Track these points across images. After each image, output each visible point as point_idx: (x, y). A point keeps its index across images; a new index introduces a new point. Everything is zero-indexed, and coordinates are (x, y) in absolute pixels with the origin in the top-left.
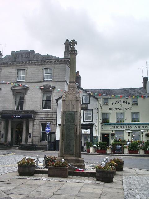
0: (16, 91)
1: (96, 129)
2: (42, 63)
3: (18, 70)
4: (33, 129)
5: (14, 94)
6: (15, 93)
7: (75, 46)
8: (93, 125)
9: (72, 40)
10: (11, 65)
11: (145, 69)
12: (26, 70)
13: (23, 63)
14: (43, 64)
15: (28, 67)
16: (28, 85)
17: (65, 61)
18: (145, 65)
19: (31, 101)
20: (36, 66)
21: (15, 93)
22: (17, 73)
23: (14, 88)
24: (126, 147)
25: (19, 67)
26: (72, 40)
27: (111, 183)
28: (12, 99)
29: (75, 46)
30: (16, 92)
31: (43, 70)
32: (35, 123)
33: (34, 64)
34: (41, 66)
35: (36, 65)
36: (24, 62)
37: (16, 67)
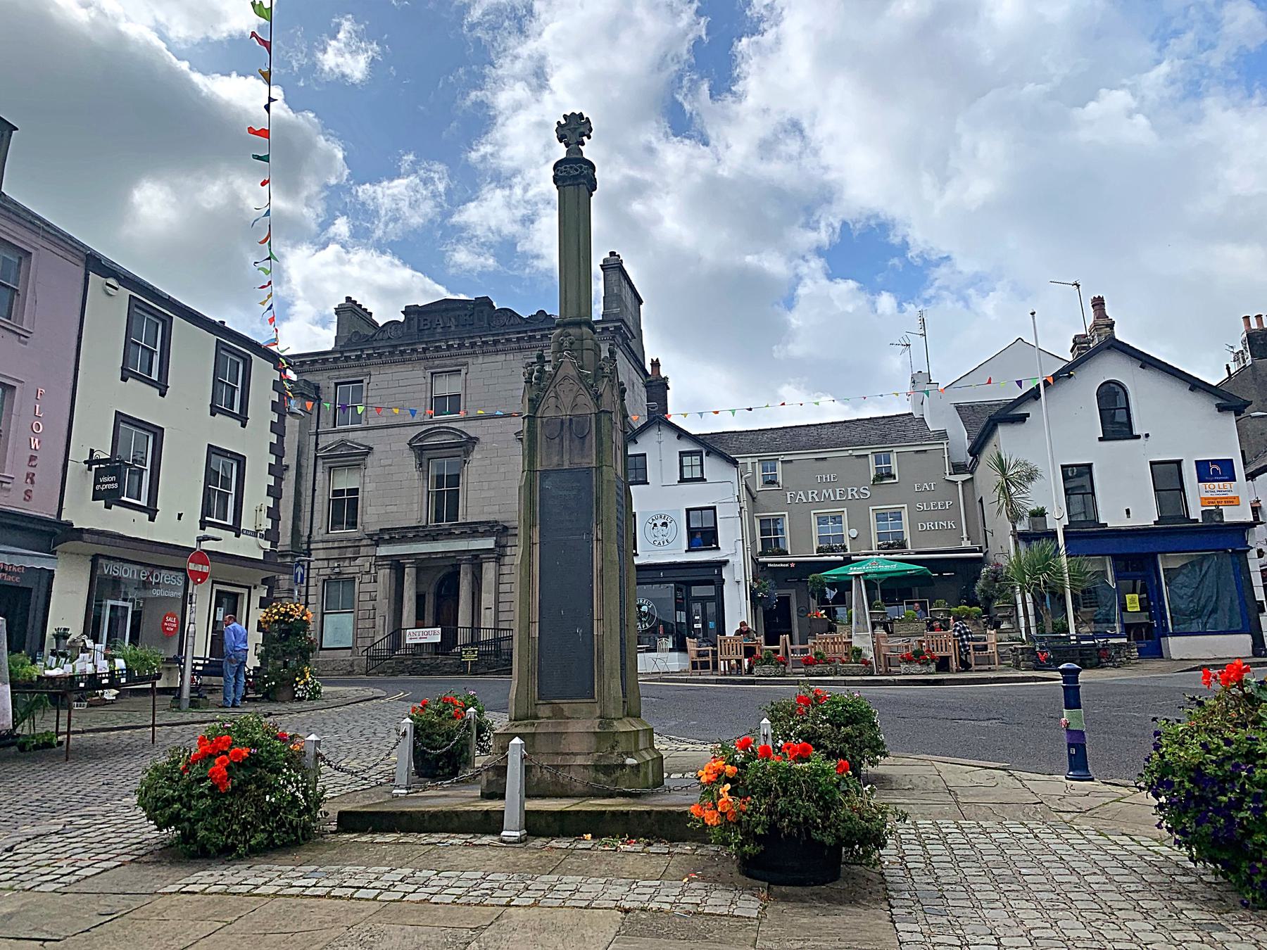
0: (428, 454)
1: (737, 579)
2: (522, 344)
3: (432, 374)
4: (497, 593)
5: (421, 465)
6: (425, 461)
7: (583, 144)
8: (725, 563)
9: (565, 116)
10: (340, 364)
11: (917, 342)
12: (463, 372)
13: (449, 347)
14: (527, 345)
15: (470, 361)
16: (472, 429)
17: (607, 329)
18: (917, 328)
19: (486, 485)
20: (501, 357)
21: (425, 461)
22: (429, 385)
23: (420, 440)
24: (472, 36)
25: (342, 373)
26: (565, 116)
27: (852, 899)
28: (417, 483)
29: (583, 144)
30: (430, 456)
31: (429, 381)
32: (505, 570)
33: (493, 349)
34: (519, 356)
35: (497, 352)
36: (455, 343)
37: (424, 363)
